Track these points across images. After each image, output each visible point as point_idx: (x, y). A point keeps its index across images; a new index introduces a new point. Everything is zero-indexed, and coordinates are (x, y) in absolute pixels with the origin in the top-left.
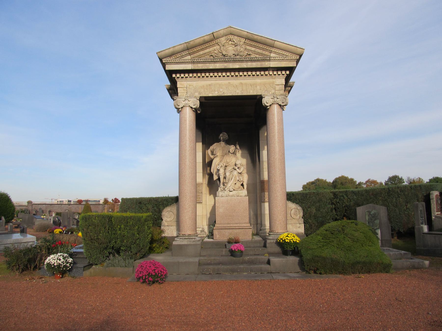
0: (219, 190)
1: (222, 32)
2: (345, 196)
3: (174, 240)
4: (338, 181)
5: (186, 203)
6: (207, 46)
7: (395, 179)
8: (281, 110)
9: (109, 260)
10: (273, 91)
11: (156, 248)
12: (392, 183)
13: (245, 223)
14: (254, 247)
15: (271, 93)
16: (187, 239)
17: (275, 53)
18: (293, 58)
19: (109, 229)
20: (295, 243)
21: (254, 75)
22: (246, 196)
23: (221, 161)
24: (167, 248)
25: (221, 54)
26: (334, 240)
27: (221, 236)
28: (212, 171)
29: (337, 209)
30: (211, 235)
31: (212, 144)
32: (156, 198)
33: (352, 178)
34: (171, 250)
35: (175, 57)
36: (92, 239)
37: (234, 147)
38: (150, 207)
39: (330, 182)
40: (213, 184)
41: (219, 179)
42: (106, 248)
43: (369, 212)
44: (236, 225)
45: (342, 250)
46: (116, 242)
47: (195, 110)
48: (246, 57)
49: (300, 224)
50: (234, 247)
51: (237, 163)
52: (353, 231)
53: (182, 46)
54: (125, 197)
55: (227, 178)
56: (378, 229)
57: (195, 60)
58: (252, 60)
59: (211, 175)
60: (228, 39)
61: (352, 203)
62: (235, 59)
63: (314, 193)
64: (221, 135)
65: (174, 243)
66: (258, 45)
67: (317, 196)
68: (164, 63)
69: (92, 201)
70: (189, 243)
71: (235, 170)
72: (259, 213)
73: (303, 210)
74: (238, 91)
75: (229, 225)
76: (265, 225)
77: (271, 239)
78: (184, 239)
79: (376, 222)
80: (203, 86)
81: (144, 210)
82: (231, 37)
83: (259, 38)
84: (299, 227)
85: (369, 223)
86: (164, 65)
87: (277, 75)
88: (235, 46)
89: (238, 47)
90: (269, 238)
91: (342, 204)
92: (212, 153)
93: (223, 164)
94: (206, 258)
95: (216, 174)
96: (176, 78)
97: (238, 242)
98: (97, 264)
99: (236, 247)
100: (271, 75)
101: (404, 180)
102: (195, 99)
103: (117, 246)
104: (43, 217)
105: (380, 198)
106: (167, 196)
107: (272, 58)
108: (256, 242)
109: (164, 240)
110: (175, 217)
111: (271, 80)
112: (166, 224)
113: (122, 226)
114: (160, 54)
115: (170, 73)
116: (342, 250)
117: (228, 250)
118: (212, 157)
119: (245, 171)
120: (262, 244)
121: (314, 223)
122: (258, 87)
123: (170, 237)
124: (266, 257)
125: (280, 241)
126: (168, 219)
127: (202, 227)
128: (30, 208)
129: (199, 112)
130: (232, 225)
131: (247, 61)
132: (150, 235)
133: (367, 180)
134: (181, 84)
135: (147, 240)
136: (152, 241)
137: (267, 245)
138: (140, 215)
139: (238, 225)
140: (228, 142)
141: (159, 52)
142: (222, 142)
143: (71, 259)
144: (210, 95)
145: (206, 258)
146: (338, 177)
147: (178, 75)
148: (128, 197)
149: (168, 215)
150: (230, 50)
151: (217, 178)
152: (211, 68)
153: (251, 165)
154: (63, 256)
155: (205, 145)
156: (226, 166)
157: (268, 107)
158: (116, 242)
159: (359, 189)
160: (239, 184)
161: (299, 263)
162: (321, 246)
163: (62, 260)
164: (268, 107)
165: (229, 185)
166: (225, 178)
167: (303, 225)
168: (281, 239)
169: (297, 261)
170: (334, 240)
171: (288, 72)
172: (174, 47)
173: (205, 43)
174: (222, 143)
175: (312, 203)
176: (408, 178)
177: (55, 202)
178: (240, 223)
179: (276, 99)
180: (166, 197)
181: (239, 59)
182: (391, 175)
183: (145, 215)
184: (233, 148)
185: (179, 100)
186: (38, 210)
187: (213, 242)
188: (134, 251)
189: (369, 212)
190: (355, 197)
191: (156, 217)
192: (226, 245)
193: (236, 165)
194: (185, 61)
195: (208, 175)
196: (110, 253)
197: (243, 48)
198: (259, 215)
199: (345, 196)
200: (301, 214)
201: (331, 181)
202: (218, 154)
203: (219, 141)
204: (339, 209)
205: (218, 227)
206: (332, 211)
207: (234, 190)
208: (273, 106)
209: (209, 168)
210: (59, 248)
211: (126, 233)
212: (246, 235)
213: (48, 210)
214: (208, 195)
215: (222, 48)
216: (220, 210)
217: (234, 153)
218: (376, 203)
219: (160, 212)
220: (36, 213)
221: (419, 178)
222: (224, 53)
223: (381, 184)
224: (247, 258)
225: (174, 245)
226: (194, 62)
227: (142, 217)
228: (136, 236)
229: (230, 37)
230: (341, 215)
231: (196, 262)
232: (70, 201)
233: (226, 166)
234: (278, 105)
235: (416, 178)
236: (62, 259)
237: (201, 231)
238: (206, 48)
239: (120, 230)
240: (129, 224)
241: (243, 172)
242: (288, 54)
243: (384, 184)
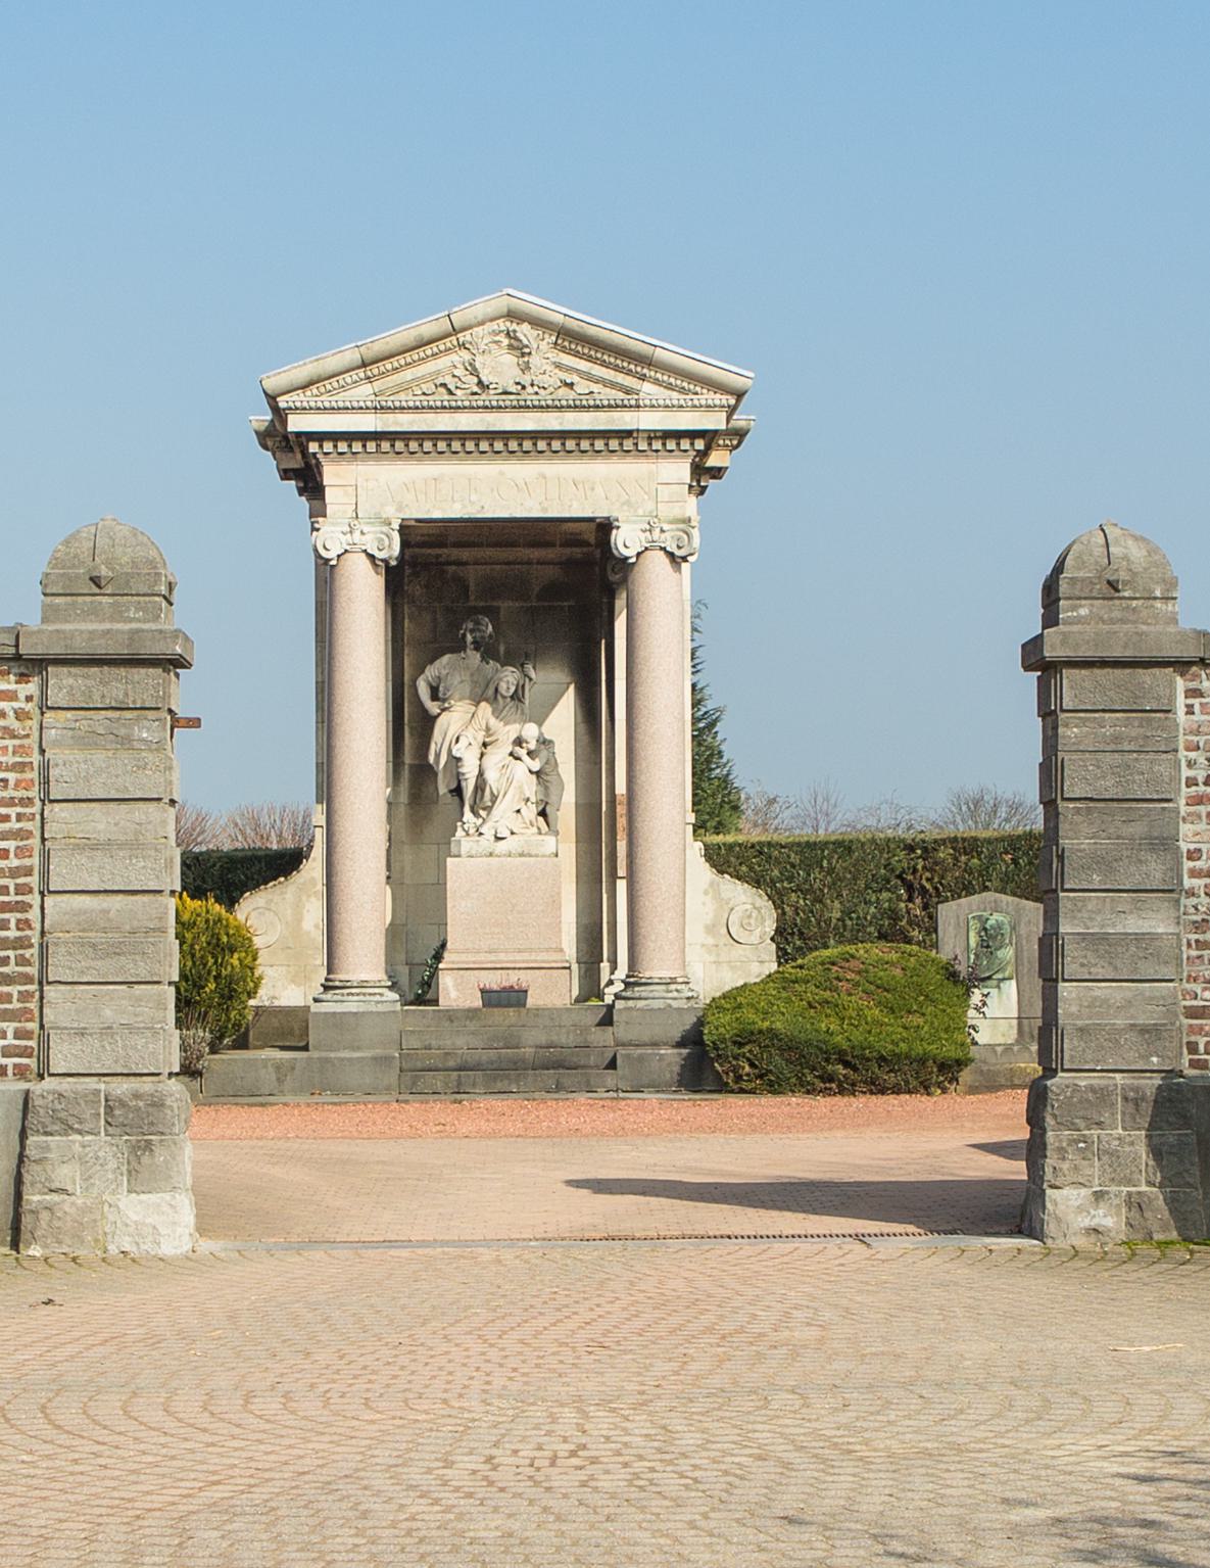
10: (650, 506)
17: (657, 382)
37: (518, 674)
44: (518, 957)
56: (1010, 978)
70: (362, 1008)
71: (518, 758)
75: (492, 957)
130: (502, 956)
139: (526, 956)
144: (437, 514)
147: (328, 446)
156: (485, 745)
171: (700, 444)
174: (474, 657)
178: (531, 950)
200: (770, 927)
203: (458, 647)
212: (554, 992)
229: (508, 324)
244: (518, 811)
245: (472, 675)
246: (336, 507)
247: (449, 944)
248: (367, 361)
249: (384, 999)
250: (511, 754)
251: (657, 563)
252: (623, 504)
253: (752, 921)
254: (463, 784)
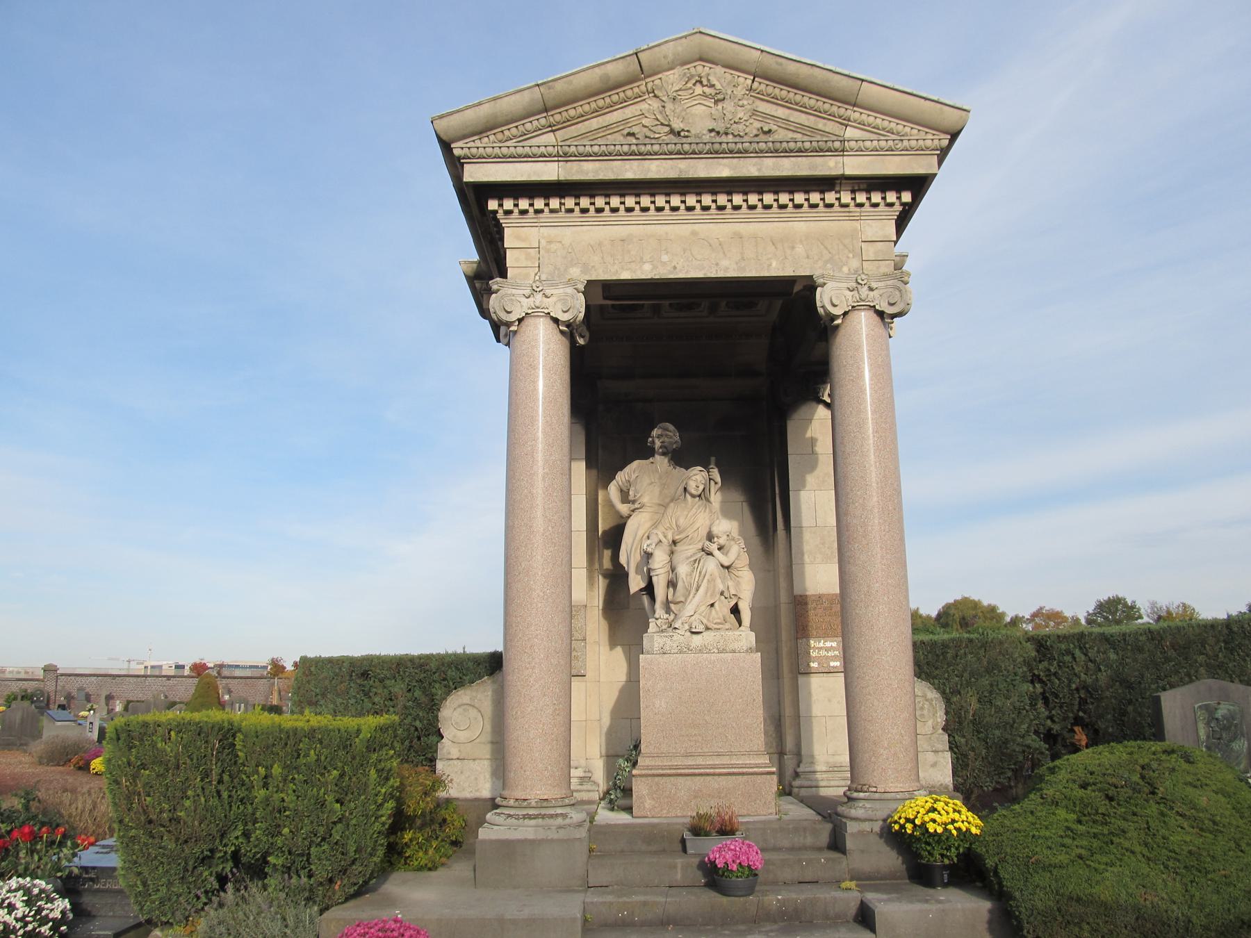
0: (652, 627)
1: (669, 50)
2: (1077, 653)
3: (481, 822)
4: (952, 612)
5: (531, 677)
6: (615, 98)
7: (1113, 608)
8: (880, 329)
9: (221, 905)
10: (855, 263)
11: (414, 846)
12: (1106, 618)
13: (749, 753)
14: (792, 849)
15: (845, 269)
16: (536, 817)
17: (862, 125)
18: (929, 143)
19: (220, 782)
20: (964, 835)
21: (783, 207)
22: (750, 650)
23: (655, 525)
24: (455, 843)
25: (667, 129)
26: (1124, 824)
27: (661, 803)
28: (623, 560)
29: (1051, 698)
30: (620, 793)
32: (420, 657)
33: (993, 603)
34: (471, 853)
35: (500, 136)
36: (150, 822)
38: (398, 688)
39: (929, 617)
40: (627, 607)
41: (649, 589)
42: (204, 860)
43: (1211, 711)
44: (717, 761)
45: (1166, 867)
46: (246, 835)
47: (569, 331)
48: (757, 139)
49: (936, 752)
50: (715, 848)
51: (715, 530)
52: (1189, 789)
53: (527, 96)
54: (311, 655)
55: (680, 585)
57: (573, 149)
58: (778, 152)
59: (617, 577)
60: (692, 76)
61: (1103, 677)
62: (717, 146)
63: (971, 641)
64: (655, 432)
65: (484, 833)
66: (798, 98)
67: (982, 652)
68: (459, 158)
69: (244, 667)
70: (541, 835)
72: (788, 711)
73: (948, 702)
74: (725, 263)
75: (690, 762)
76: (812, 756)
77: (862, 822)
78: (525, 817)
79: (1236, 746)
80: (600, 244)
81: (376, 700)
82: (701, 69)
83: (805, 70)
84: (934, 765)
85: (1208, 748)
86: (455, 165)
87: (867, 208)
88: (716, 102)
89: (728, 106)
90: (853, 813)
91: (1070, 681)
92: (625, 497)
93: (664, 534)
94: (610, 898)
95: (638, 570)
96: (500, 215)
97: (732, 832)
98: (168, 924)
99: (729, 855)
100: (847, 206)
101: (1142, 611)
102: (570, 290)
103: (249, 852)
104: (83, 713)
105: (1201, 658)
106: (460, 651)
107: (853, 144)
108: (799, 828)
109: (443, 813)
110: (488, 728)
111: (848, 225)
112: (455, 753)
113: (277, 770)
114: (442, 125)
115: (478, 202)
116: (1166, 867)
117: (696, 861)
118: (623, 509)
119: (745, 559)
120: (824, 838)
121: (973, 749)
122: (800, 249)
123: (466, 800)
124: (848, 897)
125: (903, 827)
126: (463, 736)
127: (583, 762)
128: (50, 687)
129: (581, 341)
130: (700, 761)
131: (759, 153)
132: (391, 804)
133: (1034, 609)
134: (518, 238)
135: (377, 826)
136: (400, 821)
137: (850, 844)
138: (348, 722)
139: (725, 760)
140: (681, 458)
141: (441, 117)
142: (657, 457)
143: (65, 904)
144: (626, 275)
145: (610, 898)
146: (952, 601)
147: (508, 204)
148: (326, 654)
149: (462, 719)
150: (698, 117)
151: (643, 585)
152: (629, 175)
153: (756, 541)
154: (27, 891)
155: (594, 472)
157: (838, 321)
158: (246, 835)
159: (1123, 628)
160: (723, 608)
161: (990, 922)
162: (1083, 852)
163: (21, 910)
164: (838, 321)
165: (689, 609)
166: (672, 584)
167: (948, 755)
168: (908, 820)
169: (985, 916)
170: (1124, 824)
171: (907, 197)
172: (495, 99)
173: (609, 89)
174: (661, 462)
175: (966, 675)
176: (1153, 605)
177: (138, 669)
179: (864, 291)
180: (455, 655)
181: (732, 146)
182: (1104, 597)
183: (370, 722)
184: (699, 477)
185: (510, 291)
186: (74, 693)
187: (626, 826)
188: (321, 870)
189: (1211, 711)
190: (1113, 656)
191: (418, 724)
192: (683, 841)
193: (710, 537)
194: (535, 150)
195: (605, 576)
196: (222, 880)
197: (743, 109)
198: (788, 723)
199: (1077, 653)
200: (941, 717)
201: (934, 614)
202: (645, 500)
203: (647, 453)
204: (1057, 696)
205: (648, 768)
206: (1033, 706)
207: (707, 629)
208: (853, 316)
209: (607, 554)
210: (22, 854)
211: (290, 798)
212: (757, 803)
213: (104, 693)
214: (604, 648)
215: (669, 106)
216: (657, 703)
217: (703, 496)
218: (1189, 675)
219: (433, 707)
220: (69, 702)
221: (1184, 605)
222: (677, 125)
223: (1076, 621)
224: (774, 899)
225: (484, 841)
226: (565, 154)
227: (359, 731)
228: (332, 811)
229: (700, 69)
230: (1065, 719)
231: (574, 920)
232: (183, 667)
233: (674, 543)
234: (871, 313)
236: (19, 905)
237: (583, 780)
238: (611, 108)
239: (266, 786)
240: (302, 760)
241: (738, 564)
242: (907, 130)
243: (1083, 622)
244: (712, 605)
245: (660, 478)
246: (517, 271)
247: (643, 747)
248: (549, 104)
249: (568, 821)
250: (703, 550)
251: (864, 322)
252: (826, 262)
253: (925, 712)
254: (654, 579)
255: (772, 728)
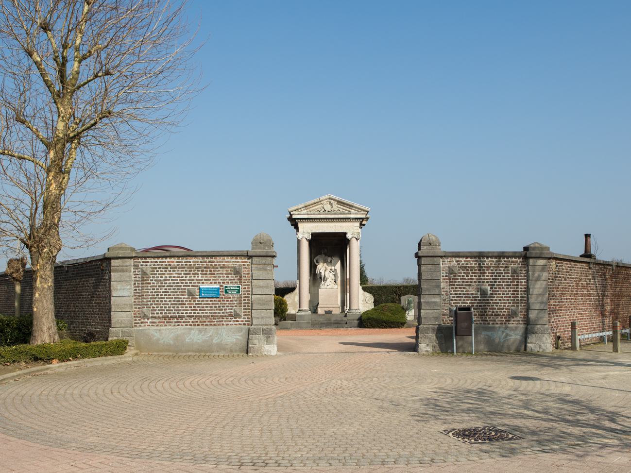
10: (353, 230)
17: (354, 210)
31: (317, 255)
147: (299, 221)
150: (328, 207)
189: (408, 299)
200: (373, 300)
203: (321, 254)
212: (337, 311)
235: (290, 281)
255: (89, 260)
